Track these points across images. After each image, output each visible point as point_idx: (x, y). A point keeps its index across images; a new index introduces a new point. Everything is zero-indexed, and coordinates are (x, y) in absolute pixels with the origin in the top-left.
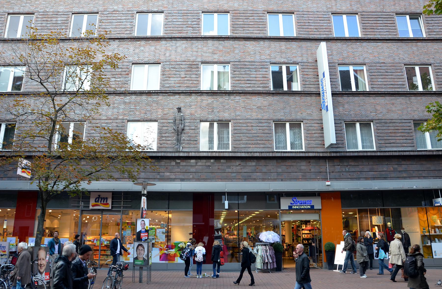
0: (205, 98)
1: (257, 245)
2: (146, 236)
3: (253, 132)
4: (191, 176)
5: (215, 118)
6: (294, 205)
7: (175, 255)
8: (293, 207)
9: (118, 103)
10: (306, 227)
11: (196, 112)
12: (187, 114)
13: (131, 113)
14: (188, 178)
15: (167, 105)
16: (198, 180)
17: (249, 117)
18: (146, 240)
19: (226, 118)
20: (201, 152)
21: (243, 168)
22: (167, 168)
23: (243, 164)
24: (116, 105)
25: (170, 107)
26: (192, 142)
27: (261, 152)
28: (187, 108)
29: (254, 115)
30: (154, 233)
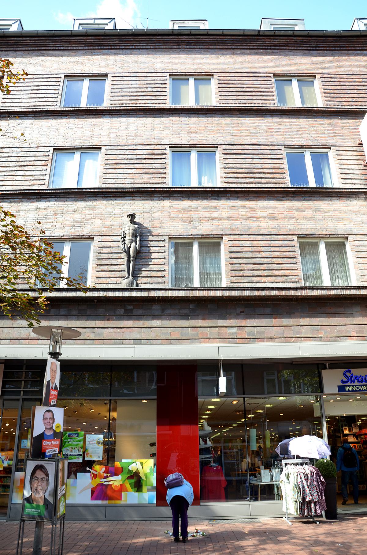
1: (286, 464)
2: (55, 446)
6: (349, 384)
7: (122, 488)
8: (347, 388)
10: (350, 430)
18: (54, 455)
25: (116, 216)
30: (82, 443)
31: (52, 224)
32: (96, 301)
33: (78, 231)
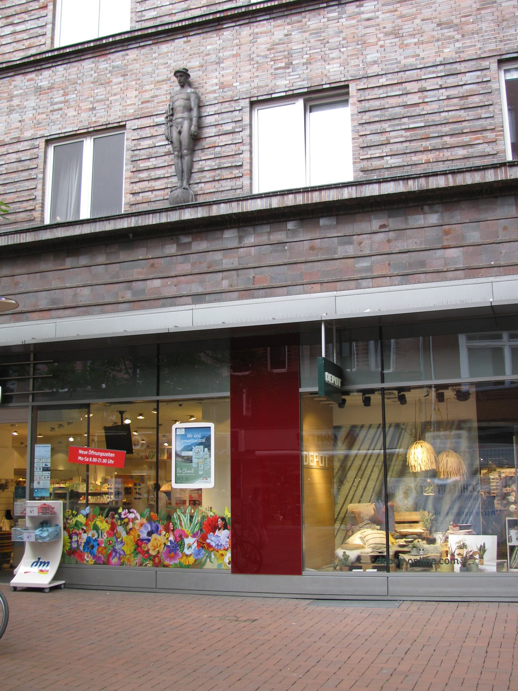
0: (264, 29)
3: (428, 108)
4: (225, 284)
5: (299, 84)
9: (21, 95)
11: (237, 75)
12: (211, 89)
13: (56, 116)
14: (214, 289)
15: (151, 74)
16: (247, 292)
17: (412, 60)
19: (333, 79)
20: (260, 196)
21: (396, 239)
22: (152, 265)
23: (393, 223)
24: (16, 102)
25: (160, 78)
26: (226, 174)
27: (453, 172)
28: (210, 68)
29: (429, 54)
31: (60, 112)
32: (131, 235)
33: (102, 117)
